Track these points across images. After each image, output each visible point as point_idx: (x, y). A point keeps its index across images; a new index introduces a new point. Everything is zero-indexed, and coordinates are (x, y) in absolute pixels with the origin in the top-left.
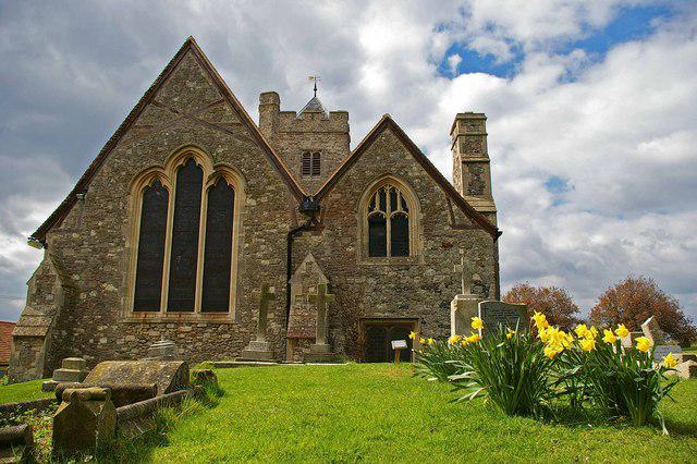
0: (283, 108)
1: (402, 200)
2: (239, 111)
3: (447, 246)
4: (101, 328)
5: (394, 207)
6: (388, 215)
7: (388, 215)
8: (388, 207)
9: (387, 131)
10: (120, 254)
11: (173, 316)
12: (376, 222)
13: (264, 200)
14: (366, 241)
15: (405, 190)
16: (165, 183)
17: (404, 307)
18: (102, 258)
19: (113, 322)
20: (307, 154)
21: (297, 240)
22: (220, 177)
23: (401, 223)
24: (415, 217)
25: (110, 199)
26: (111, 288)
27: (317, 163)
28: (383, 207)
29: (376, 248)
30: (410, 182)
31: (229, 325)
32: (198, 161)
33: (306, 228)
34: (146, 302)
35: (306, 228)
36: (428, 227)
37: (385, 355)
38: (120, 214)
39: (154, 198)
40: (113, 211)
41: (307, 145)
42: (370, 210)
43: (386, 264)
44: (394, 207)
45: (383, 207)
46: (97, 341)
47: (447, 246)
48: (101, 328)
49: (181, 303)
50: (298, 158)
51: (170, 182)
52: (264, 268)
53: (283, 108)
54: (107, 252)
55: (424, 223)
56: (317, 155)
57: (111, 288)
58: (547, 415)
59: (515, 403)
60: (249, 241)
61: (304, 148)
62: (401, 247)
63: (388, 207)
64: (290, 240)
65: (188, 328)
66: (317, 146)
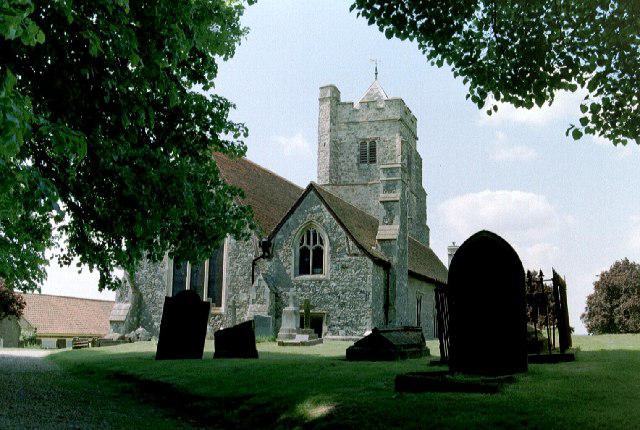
0: (342, 101)
1: (320, 238)
3: (344, 267)
5: (315, 242)
6: (311, 248)
7: (311, 248)
8: (312, 242)
9: (312, 192)
12: (304, 253)
14: (298, 264)
15: (321, 230)
20: (363, 143)
23: (319, 253)
24: (326, 248)
27: (373, 151)
28: (308, 243)
31: (221, 315)
36: (333, 253)
41: (362, 134)
42: (301, 245)
44: (315, 242)
45: (308, 243)
47: (344, 267)
53: (342, 101)
58: (632, 332)
59: (599, 319)
61: (361, 137)
62: (318, 264)
63: (312, 242)
64: (254, 264)
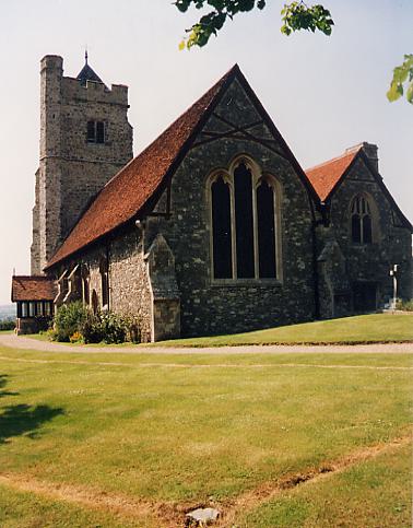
2: (106, 87)
4: (195, 292)
5: (364, 212)
10: (202, 235)
11: (244, 281)
13: (295, 200)
16: (226, 180)
17: (373, 275)
18: (190, 238)
19: (203, 287)
20: (91, 123)
21: (316, 229)
22: (264, 180)
23: (367, 220)
25: (189, 190)
26: (198, 260)
29: (356, 238)
30: (373, 194)
32: (248, 166)
33: (320, 222)
34: (222, 271)
35: (320, 222)
37: (68, 341)
38: (202, 199)
39: (220, 190)
40: (193, 200)
41: (91, 114)
43: (362, 248)
44: (364, 212)
46: (192, 300)
48: (195, 292)
49: (245, 271)
50: (84, 124)
51: (230, 181)
52: (298, 247)
54: (192, 232)
55: (381, 222)
56: (100, 125)
57: (198, 260)
60: (287, 229)
62: (368, 238)
65: (254, 290)
66: (101, 116)
